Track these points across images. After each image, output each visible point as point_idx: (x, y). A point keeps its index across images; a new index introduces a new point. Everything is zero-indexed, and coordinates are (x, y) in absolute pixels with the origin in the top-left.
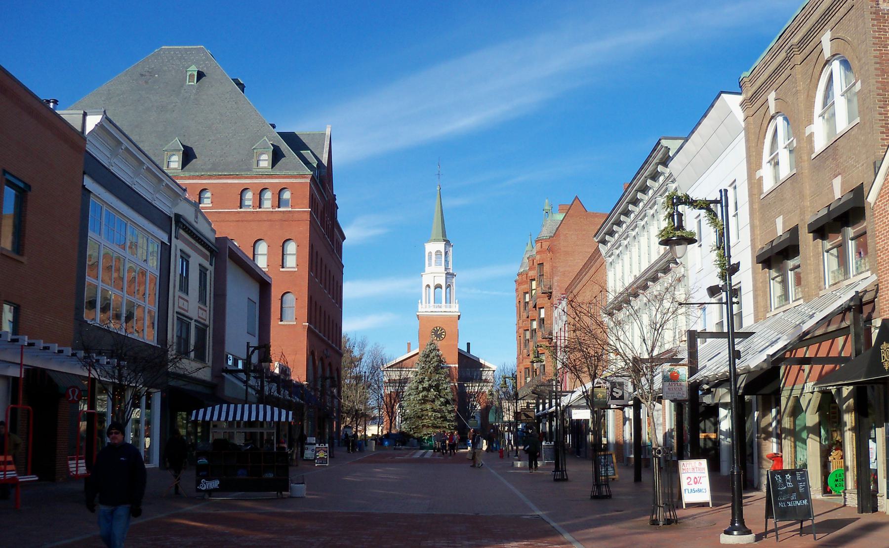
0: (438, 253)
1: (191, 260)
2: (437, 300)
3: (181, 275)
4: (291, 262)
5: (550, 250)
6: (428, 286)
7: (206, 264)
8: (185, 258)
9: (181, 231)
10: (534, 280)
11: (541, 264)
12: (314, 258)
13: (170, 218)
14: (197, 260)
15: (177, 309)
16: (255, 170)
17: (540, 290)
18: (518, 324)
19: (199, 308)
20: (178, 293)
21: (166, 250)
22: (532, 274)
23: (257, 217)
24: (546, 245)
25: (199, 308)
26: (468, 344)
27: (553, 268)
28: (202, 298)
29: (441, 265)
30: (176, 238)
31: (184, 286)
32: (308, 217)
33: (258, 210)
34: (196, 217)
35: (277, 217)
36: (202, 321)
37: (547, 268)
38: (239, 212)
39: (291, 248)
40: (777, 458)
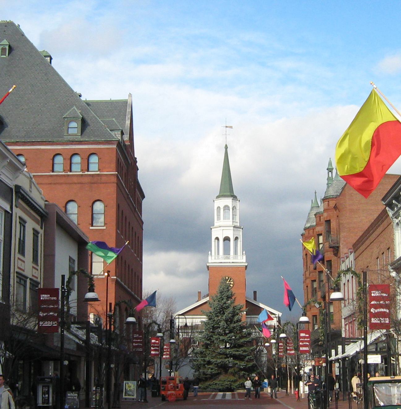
0: (226, 208)
1: (27, 225)
2: (227, 251)
3: (20, 239)
4: (100, 221)
5: (336, 207)
6: (217, 239)
7: (38, 228)
8: (23, 222)
9: (20, 201)
10: (321, 234)
11: (328, 222)
12: (120, 215)
13: (11, 189)
14: (31, 225)
15: (17, 270)
16: (67, 138)
17: (327, 245)
18: (305, 274)
19: (33, 267)
20: (18, 256)
21: (8, 216)
22: (319, 229)
23: (66, 180)
24: (332, 203)
25: (33, 267)
26: (255, 293)
27: (339, 225)
28: (35, 260)
29: (229, 219)
30: (16, 207)
31: (22, 251)
32: (114, 180)
33: (69, 173)
34: (31, 187)
35: (86, 180)
36: (35, 279)
37: (333, 224)
38: (51, 176)
39: (99, 207)
40: (305, 373)
